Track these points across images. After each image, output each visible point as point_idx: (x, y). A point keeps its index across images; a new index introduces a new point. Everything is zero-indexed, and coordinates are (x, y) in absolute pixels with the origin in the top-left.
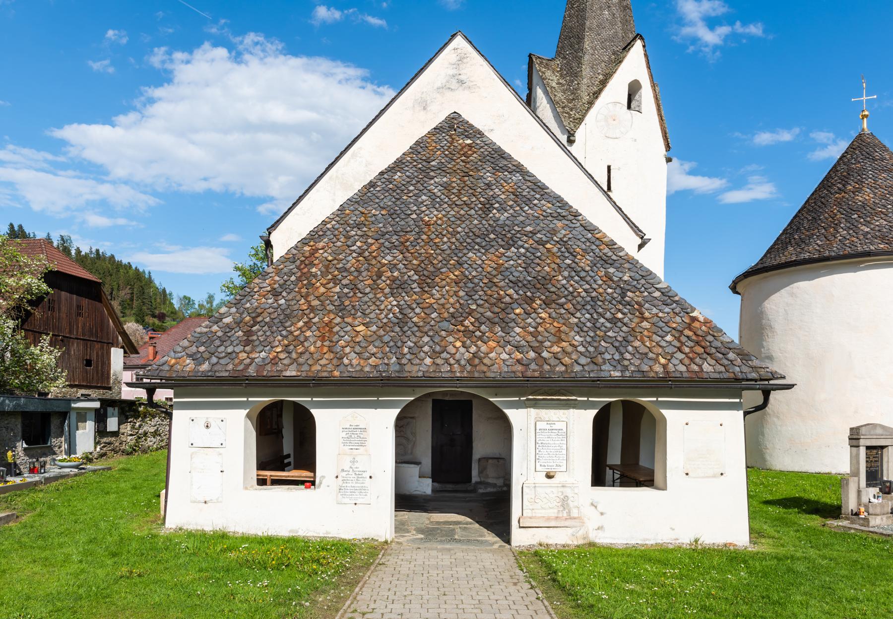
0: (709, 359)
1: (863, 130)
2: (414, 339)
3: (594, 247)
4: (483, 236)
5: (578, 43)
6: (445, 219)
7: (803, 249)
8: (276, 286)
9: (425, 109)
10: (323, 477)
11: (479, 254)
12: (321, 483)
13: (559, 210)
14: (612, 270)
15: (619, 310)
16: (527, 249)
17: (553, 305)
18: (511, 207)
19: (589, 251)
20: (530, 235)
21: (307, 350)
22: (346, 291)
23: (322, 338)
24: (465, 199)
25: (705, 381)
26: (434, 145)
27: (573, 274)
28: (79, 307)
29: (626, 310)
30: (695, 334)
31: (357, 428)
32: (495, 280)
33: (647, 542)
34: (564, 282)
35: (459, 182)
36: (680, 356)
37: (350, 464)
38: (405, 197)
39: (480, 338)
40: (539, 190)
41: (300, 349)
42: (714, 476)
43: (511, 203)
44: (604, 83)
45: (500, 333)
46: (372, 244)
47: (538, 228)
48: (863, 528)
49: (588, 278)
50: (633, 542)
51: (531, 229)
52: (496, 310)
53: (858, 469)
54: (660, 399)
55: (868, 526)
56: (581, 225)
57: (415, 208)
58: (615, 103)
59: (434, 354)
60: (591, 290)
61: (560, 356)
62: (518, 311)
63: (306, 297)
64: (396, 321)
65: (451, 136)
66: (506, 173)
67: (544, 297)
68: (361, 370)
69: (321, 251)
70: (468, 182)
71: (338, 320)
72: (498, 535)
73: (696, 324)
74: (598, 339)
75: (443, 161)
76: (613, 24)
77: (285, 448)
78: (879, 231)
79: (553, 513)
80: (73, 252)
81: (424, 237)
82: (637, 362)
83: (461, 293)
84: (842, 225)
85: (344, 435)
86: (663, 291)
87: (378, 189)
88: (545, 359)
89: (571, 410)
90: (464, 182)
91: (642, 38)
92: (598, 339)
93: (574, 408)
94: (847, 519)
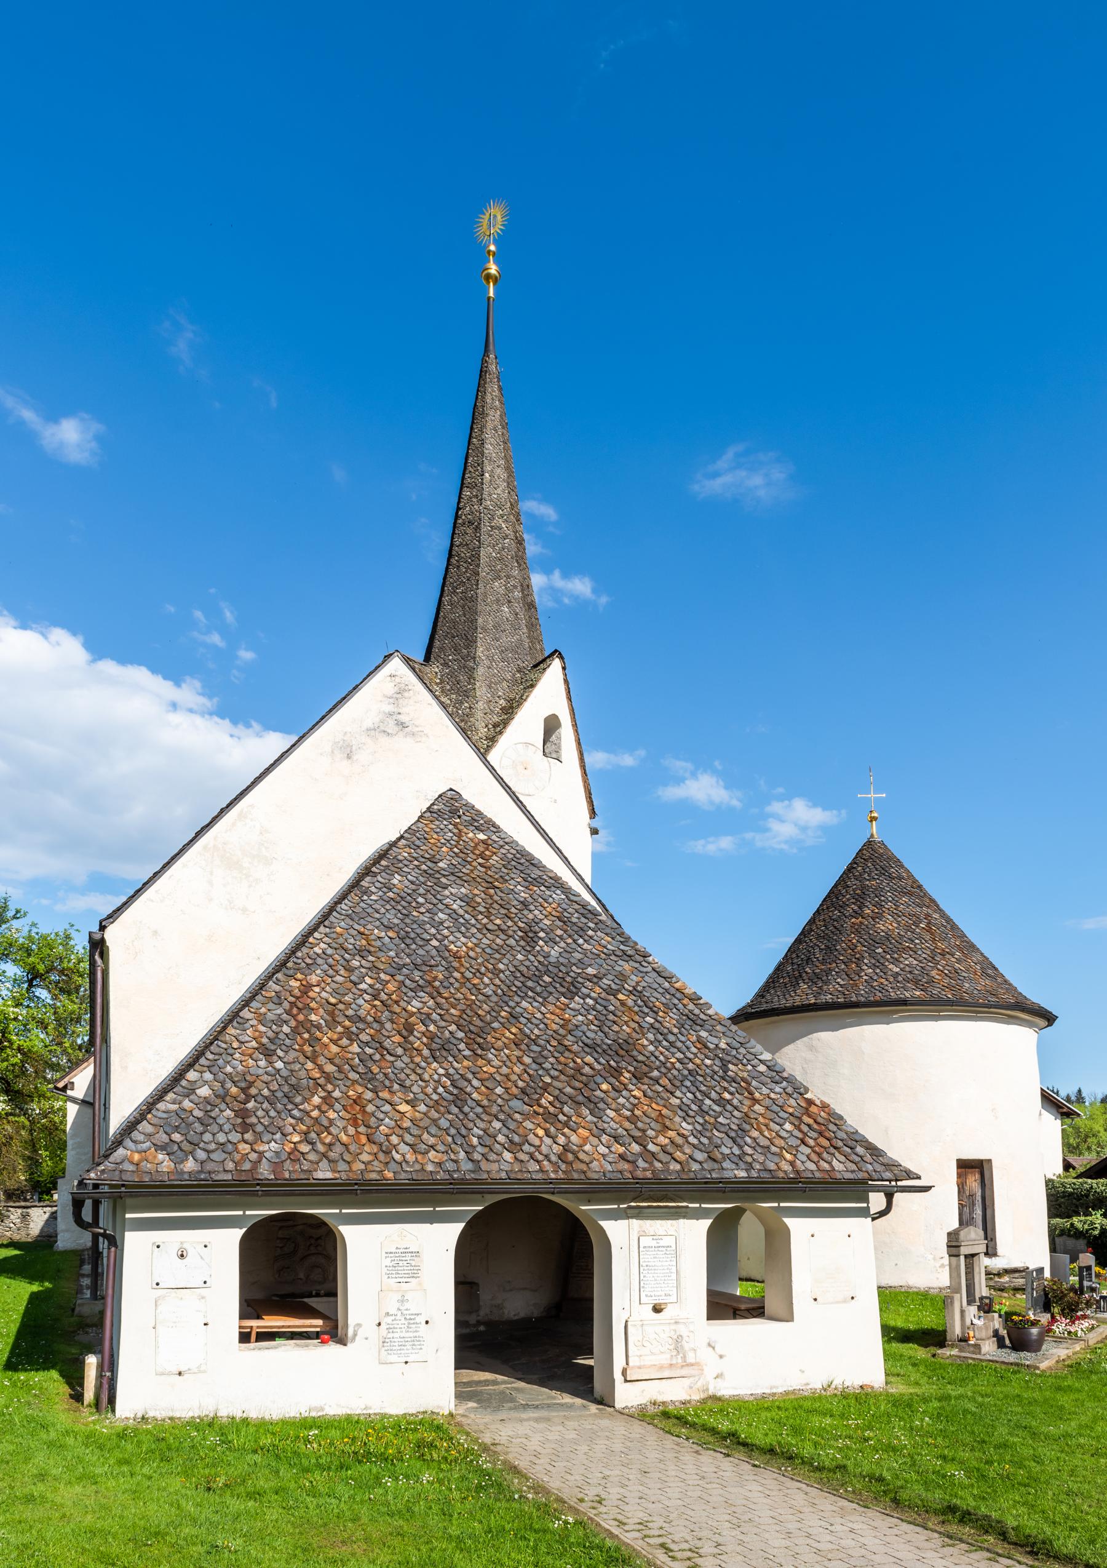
0: (837, 1154)
1: (872, 836)
2: (482, 1125)
3: (676, 1001)
4: (534, 978)
5: (467, 647)
6: (478, 950)
7: (820, 988)
8: (265, 1040)
9: (349, 757)
10: (359, 1325)
11: (535, 1004)
12: (355, 1335)
13: (622, 947)
14: (704, 1034)
15: (725, 1089)
17: (646, 1080)
18: (560, 937)
19: (671, 1006)
20: (595, 980)
22: (368, 1051)
23: (355, 1123)
24: (498, 922)
25: (837, 1182)
26: (435, 836)
27: (660, 1038)
29: (733, 1089)
30: (815, 1121)
31: (406, 1251)
32: (566, 1043)
33: (774, 1391)
34: (651, 1048)
35: (483, 895)
37: (398, 1305)
38: (415, 913)
39: (566, 1125)
40: (590, 916)
42: (845, 1301)
43: (559, 932)
45: (590, 1118)
46: (387, 982)
47: (603, 971)
48: (974, 1356)
49: (679, 1044)
50: (759, 1391)
51: (595, 972)
52: (578, 1085)
53: (960, 1283)
54: (782, 1205)
55: (980, 1353)
56: (654, 969)
57: (433, 931)
59: (514, 1147)
60: (686, 1061)
61: (670, 1149)
62: (604, 1087)
63: (313, 1059)
64: (451, 1098)
65: (455, 825)
66: (543, 888)
67: (632, 1069)
68: (423, 1169)
69: (317, 989)
70: (496, 898)
71: (369, 1095)
72: (575, 1393)
73: (813, 1109)
74: (709, 1127)
75: (453, 862)
76: (516, 628)
77: (291, 1281)
78: (910, 972)
79: (665, 1359)
81: (456, 975)
82: (761, 1158)
83: (527, 1060)
84: (866, 961)
85: (388, 1262)
86: (769, 1064)
87: (373, 897)
88: (653, 1154)
89: (681, 1221)
90: (491, 897)
91: (561, 657)
92: (709, 1127)
93: (684, 1217)
94: (952, 1346)
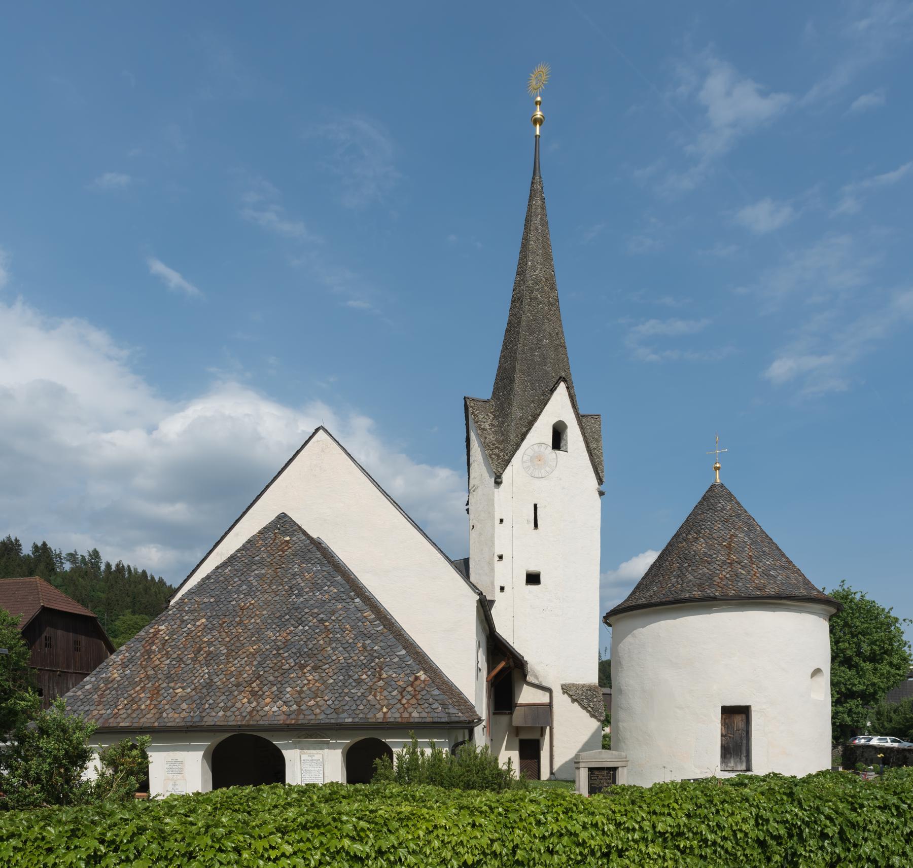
16: (310, 627)
21: (139, 708)
28: (76, 642)
36: (399, 706)
41: (135, 706)
44: (531, 424)
58: (540, 444)
59: (226, 709)
73: (418, 682)
80: (103, 567)
85: (167, 766)
91: (565, 380)
